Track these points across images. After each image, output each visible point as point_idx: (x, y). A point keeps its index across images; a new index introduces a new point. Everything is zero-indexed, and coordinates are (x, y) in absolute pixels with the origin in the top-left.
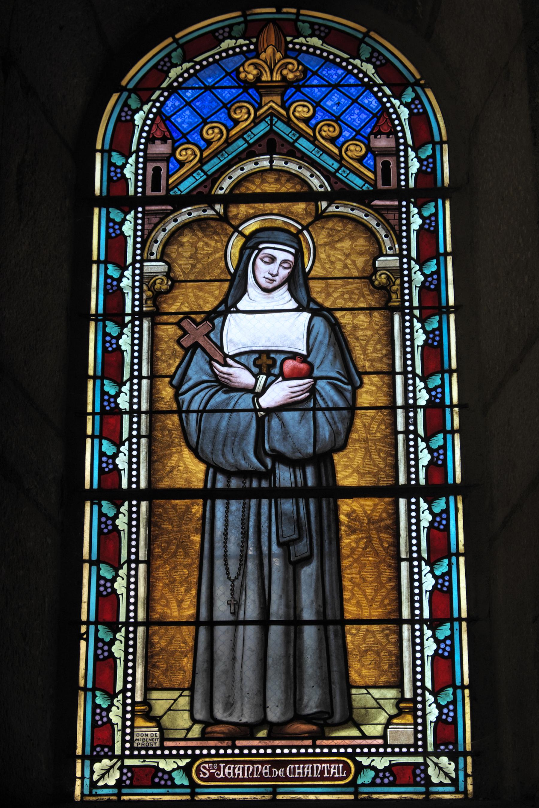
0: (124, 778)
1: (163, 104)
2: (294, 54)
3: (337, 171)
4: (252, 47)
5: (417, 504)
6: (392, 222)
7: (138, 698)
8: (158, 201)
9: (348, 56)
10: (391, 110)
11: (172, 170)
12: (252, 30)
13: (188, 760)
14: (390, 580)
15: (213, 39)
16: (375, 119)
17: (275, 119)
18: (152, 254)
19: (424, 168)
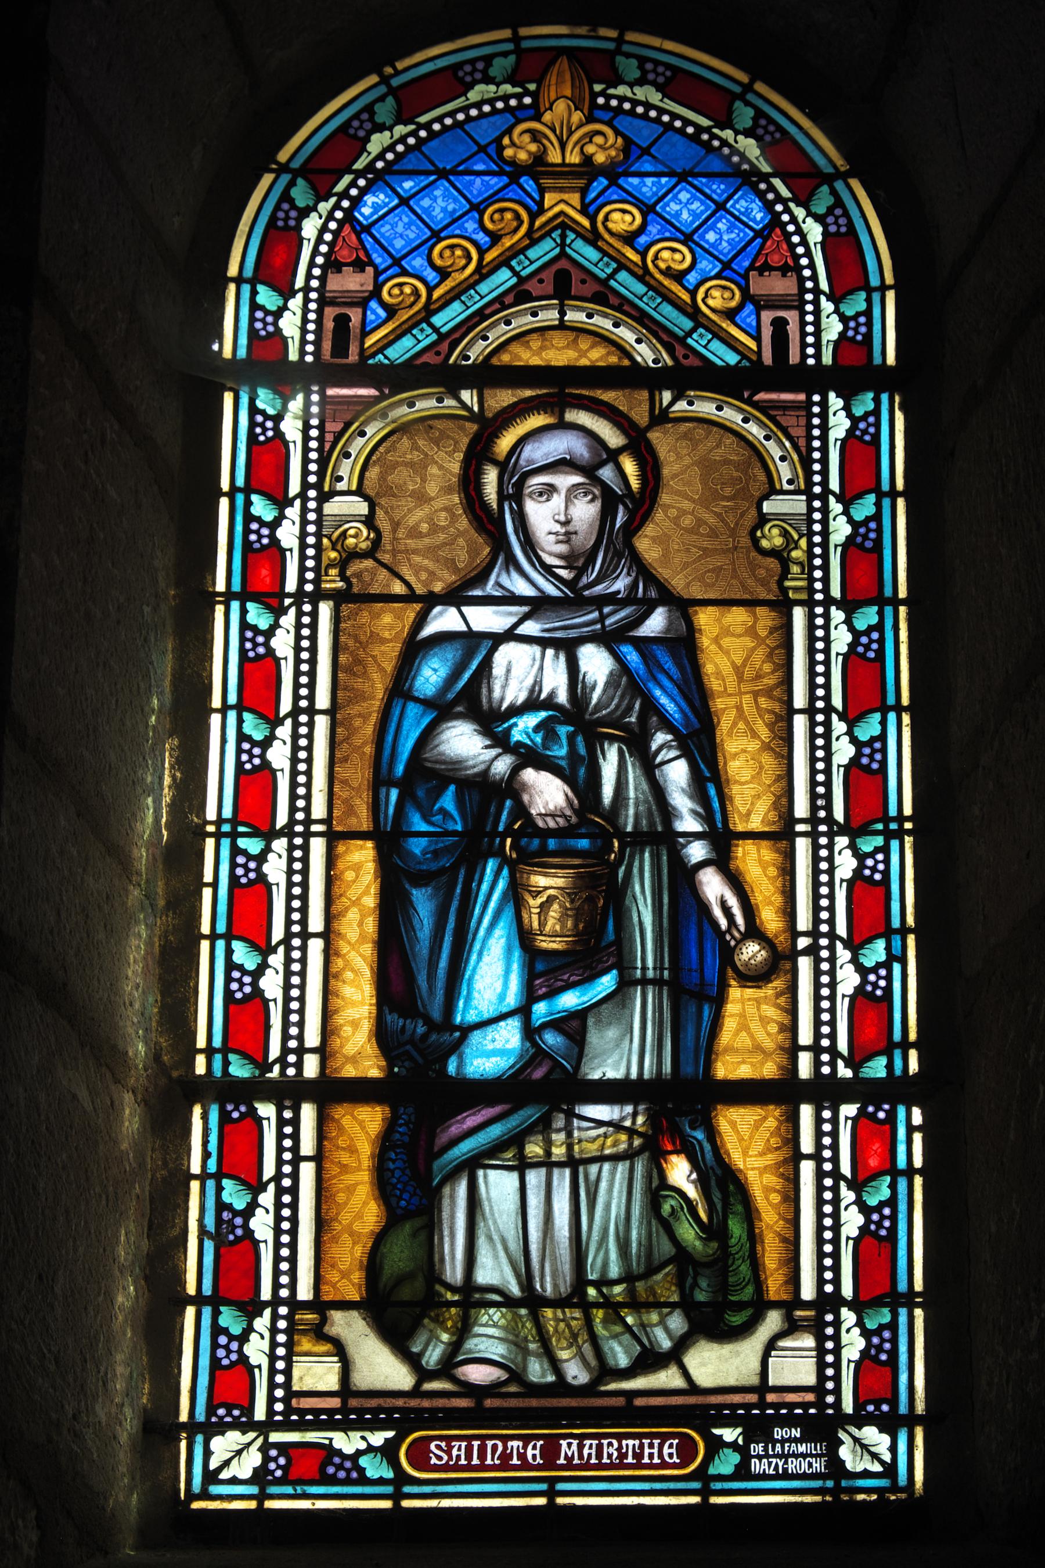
0: (272, 1466)
1: (356, 202)
2: (609, 115)
3: (689, 334)
4: (527, 100)
6: (793, 432)
10: (791, 228)
11: (372, 322)
12: (531, 67)
15: (453, 81)
16: (759, 241)
17: (571, 236)
19: (851, 333)
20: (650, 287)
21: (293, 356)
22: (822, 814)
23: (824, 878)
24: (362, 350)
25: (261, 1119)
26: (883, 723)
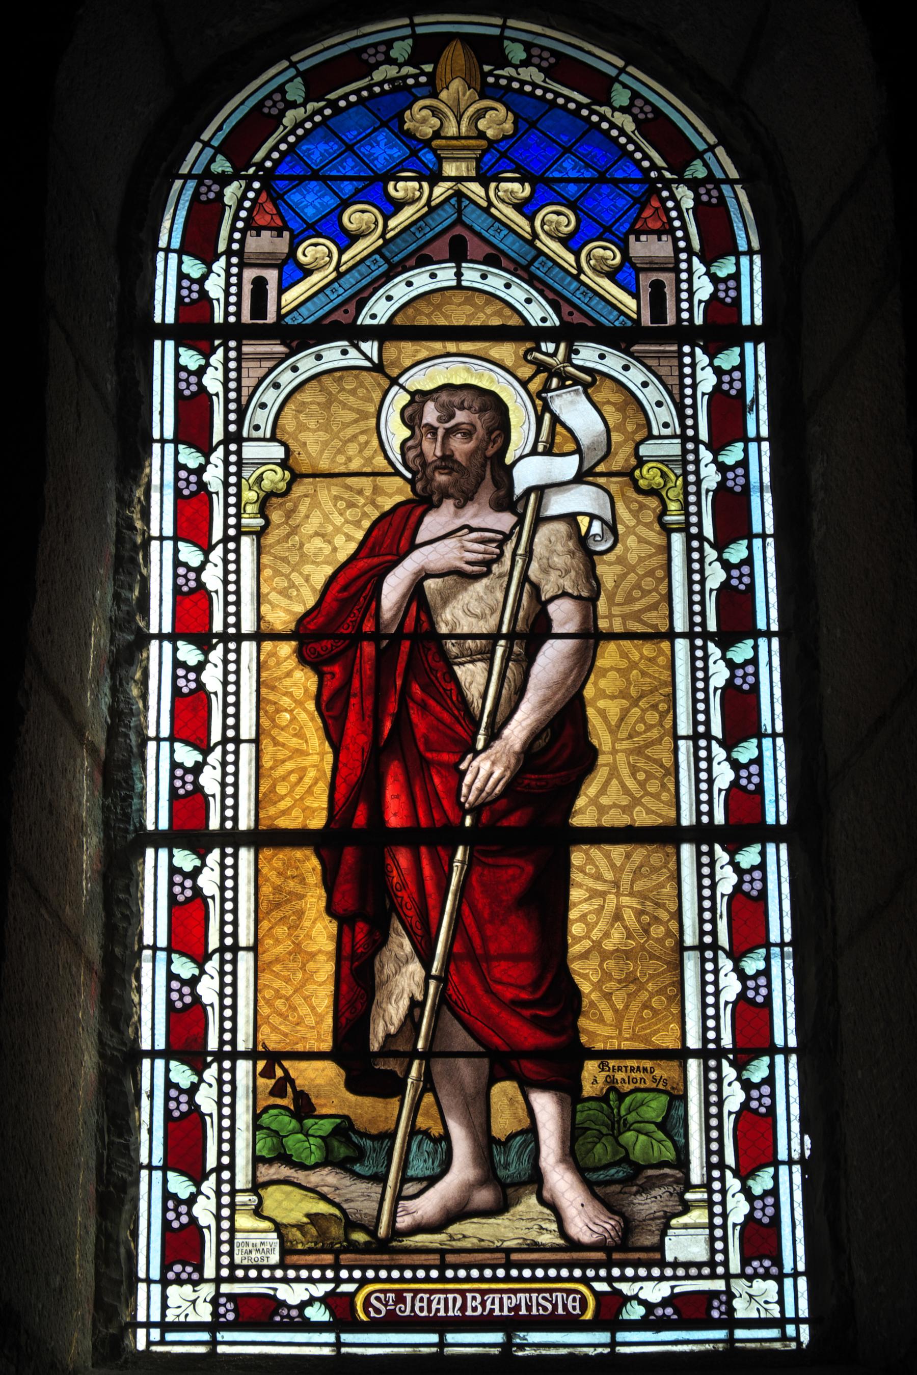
4: (423, 79)
5: (711, 854)
9: (664, 165)
16: (638, 206)
18: (257, 428)
21: (219, 318)
22: (701, 729)
23: (697, 588)
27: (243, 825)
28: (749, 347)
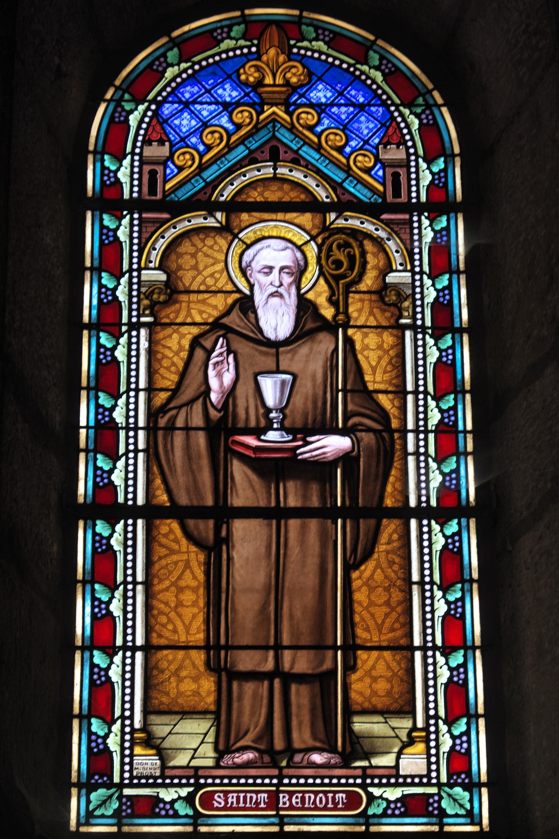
3: (344, 181)
7: (137, 725)
8: (156, 206)
13: (191, 789)
14: (399, 603)
15: (210, 38)
20: (322, 155)
21: (126, 196)
24: (164, 191)
25: (117, 486)
26: (458, 462)
27: (140, 501)
28: (452, 215)
